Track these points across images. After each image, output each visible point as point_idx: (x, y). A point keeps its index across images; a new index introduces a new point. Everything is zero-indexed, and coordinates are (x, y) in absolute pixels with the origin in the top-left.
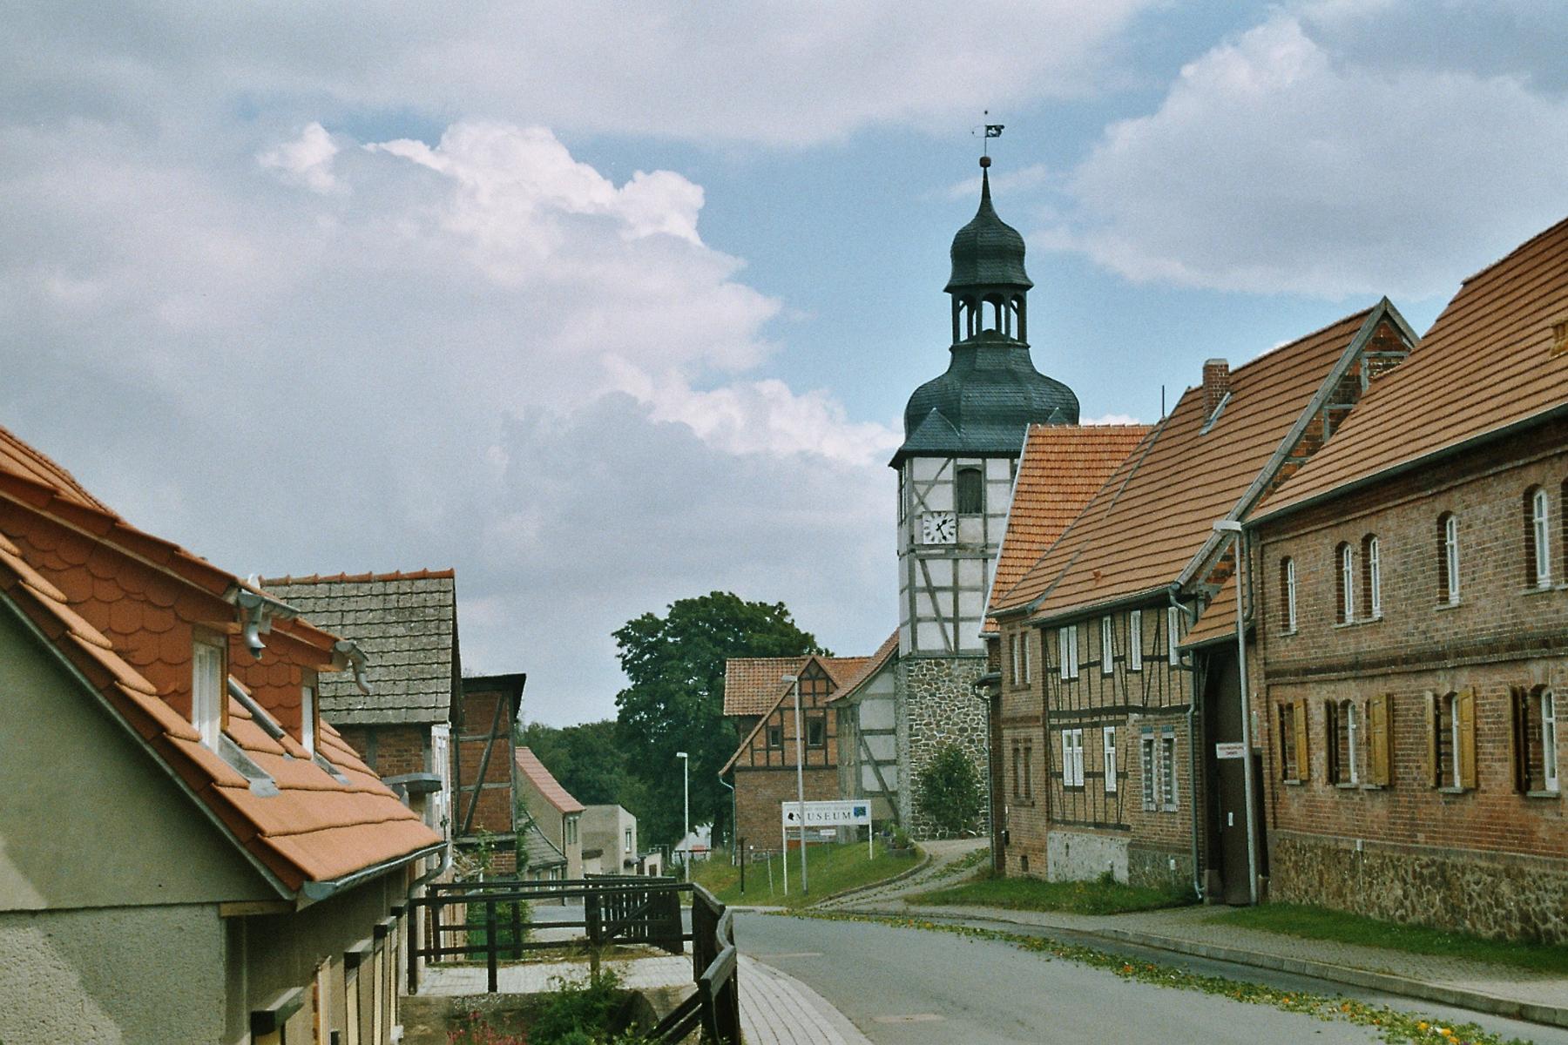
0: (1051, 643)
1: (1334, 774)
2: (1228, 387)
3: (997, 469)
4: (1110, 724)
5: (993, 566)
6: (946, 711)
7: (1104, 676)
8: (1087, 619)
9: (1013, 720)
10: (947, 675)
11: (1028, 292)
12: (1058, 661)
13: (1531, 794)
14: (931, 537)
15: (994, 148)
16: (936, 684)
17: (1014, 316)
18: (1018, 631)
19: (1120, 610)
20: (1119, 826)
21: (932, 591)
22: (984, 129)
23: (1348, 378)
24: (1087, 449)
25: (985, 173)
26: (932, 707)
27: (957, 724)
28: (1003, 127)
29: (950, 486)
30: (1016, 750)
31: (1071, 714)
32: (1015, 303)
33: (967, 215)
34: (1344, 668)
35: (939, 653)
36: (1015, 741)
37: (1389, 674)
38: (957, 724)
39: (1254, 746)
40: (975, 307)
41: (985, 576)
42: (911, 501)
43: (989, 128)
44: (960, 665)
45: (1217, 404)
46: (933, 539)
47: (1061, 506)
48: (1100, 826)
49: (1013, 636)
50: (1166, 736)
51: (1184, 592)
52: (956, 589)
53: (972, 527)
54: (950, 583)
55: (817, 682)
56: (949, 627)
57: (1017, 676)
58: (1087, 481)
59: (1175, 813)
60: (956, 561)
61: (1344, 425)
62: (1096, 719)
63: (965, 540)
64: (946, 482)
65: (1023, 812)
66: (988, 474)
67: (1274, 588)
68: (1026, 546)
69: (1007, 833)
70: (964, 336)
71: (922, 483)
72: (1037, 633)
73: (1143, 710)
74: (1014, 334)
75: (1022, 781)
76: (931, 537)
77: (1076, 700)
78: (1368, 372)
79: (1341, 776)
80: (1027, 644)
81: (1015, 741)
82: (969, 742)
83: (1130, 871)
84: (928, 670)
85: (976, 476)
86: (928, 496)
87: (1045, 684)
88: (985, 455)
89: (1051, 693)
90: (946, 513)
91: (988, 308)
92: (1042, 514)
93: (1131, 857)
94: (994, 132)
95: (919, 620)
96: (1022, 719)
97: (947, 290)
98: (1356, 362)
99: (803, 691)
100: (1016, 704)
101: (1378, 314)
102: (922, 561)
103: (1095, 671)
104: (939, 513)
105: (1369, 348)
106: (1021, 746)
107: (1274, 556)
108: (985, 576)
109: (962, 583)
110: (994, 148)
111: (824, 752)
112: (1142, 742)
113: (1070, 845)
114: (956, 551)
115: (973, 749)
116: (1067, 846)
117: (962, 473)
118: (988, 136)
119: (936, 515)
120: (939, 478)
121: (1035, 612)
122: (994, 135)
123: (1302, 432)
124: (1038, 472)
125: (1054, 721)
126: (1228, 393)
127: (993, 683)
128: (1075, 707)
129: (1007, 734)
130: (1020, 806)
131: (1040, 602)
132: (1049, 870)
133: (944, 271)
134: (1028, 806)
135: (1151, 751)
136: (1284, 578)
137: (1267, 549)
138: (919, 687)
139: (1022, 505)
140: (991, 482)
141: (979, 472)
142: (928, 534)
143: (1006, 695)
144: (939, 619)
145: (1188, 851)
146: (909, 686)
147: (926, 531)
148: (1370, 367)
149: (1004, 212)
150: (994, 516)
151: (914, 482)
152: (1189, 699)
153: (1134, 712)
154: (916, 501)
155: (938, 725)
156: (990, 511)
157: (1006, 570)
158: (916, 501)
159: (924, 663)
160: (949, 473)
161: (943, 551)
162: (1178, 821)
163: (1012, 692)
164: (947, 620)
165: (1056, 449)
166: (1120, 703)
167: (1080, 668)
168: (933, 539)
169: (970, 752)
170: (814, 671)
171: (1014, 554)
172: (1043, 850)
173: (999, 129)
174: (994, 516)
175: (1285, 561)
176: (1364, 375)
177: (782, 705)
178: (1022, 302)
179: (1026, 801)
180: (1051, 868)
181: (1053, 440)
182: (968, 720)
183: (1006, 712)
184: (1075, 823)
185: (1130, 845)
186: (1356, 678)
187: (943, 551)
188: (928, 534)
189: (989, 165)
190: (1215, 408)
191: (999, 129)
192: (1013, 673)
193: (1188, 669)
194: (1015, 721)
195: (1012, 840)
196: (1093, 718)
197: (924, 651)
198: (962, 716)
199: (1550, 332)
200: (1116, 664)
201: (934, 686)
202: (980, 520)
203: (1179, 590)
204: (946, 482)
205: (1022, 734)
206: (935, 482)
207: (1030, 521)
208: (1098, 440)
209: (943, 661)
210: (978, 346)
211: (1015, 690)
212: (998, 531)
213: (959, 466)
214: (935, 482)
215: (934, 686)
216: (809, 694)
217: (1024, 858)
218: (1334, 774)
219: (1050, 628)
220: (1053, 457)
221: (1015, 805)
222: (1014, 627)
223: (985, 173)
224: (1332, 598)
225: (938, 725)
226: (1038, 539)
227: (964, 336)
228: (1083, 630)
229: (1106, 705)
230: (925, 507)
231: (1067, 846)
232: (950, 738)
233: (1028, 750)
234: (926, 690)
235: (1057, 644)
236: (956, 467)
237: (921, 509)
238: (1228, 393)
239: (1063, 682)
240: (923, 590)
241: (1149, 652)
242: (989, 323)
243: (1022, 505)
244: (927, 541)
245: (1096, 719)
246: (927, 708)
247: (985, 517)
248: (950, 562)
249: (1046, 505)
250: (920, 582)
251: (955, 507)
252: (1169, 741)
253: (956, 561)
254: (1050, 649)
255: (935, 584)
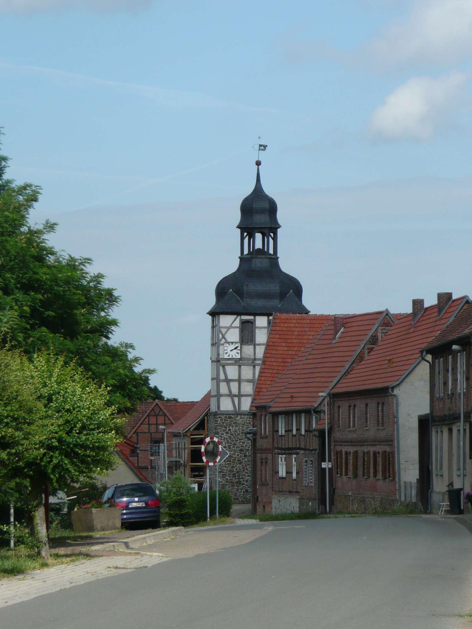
0: (276, 421)
1: (375, 475)
2: (343, 325)
3: (261, 321)
4: (295, 454)
5: (258, 369)
6: (233, 441)
7: (293, 436)
8: (288, 414)
9: (261, 450)
10: (234, 423)
11: (278, 229)
12: (278, 428)
13: (377, 478)
14: (228, 355)
15: (263, 156)
16: (229, 427)
17: (271, 241)
18: (264, 414)
19: (298, 413)
20: (297, 492)
21: (228, 381)
22: (258, 146)
23: (374, 336)
24: (300, 325)
25: (258, 169)
26: (227, 439)
27: (239, 447)
28: (267, 146)
29: (238, 330)
30: (262, 462)
31: (281, 449)
32: (272, 234)
33: (249, 189)
34: (348, 442)
35: (231, 412)
36: (261, 459)
37: (364, 445)
38: (239, 447)
39: (136, 458)
40: (251, 236)
41: (254, 374)
42: (218, 337)
43: (261, 146)
44: (241, 418)
45: (339, 332)
46: (229, 356)
47: (287, 353)
48: (290, 492)
49: (261, 415)
50: (311, 459)
51: (316, 410)
52: (239, 381)
53: (248, 350)
54: (236, 377)
55: (158, 417)
56: (236, 399)
57: (263, 432)
58: (299, 341)
59: (313, 486)
60: (240, 366)
61: (372, 353)
62: (290, 452)
63: (244, 356)
64: (236, 327)
65: (264, 488)
66: (256, 324)
67: (336, 415)
68: (271, 371)
69: (258, 497)
70: (246, 252)
71: (225, 327)
72: (271, 415)
73: (305, 449)
74: (271, 251)
75: (263, 475)
76: (228, 355)
77: (283, 444)
78: (381, 334)
79: (348, 474)
80: (267, 418)
81: (261, 459)
82: (244, 456)
83: (299, 508)
84: (225, 420)
85: (250, 324)
86: (227, 334)
87: (273, 436)
88: (255, 315)
89: (275, 440)
90: (236, 343)
91: (259, 236)
92: (278, 356)
93: (300, 503)
94: (263, 148)
95: (221, 395)
96: (264, 450)
97: (238, 227)
98: (376, 330)
99: (150, 422)
100: (261, 443)
101: (385, 314)
102: (223, 366)
103: (290, 433)
104: (232, 343)
105: (382, 326)
106: (264, 461)
107: (336, 405)
108: (254, 374)
109: (243, 377)
110: (263, 156)
111: (136, 458)
112: (304, 461)
113: (281, 500)
114: (239, 362)
115: (246, 460)
116: (279, 501)
117: (243, 323)
118: (260, 150)
119: (231, 344)
120: (232, 326)
121: (270, 407)
122: (263, 150)
123: (358, 355)
124: (277, 336)
125: (276, 451)
126: (343, 328)
127: (255, 434)
128: (283, 447)
129: (259, 456)
130: (263, 485)
131: (272, 403)
132: (273, 510)
133: (237, 217)
134: (266, 485)
135: (307, 464)
136: (339, 412)
137: (336, 402)
138: (220, 429)
139: (270, 352)
140: (258, 328)
141: (252, 323)
142: (226, 353)
143: (258, 439)
144: (231, 395)
145: (316, 500)
146: (215, 428)
147: (226, 352)
148: (381, 333)
149: (268, 190)
150: (259, 345)
151: (220, 327)
152: (317, 447)
153: (302, 450)
154: (221, 336)
155: (229, 448)
156: (257, 342)
157: (261, 382)
158: (221, 336)
159: (223, 417)
160: (237, 323)
161: (233, 362)
162: (314, 489)
163: (261, 438)
164: (235, 396)
165: (286, 325)
166: (298, 446)
167: (285, 431)
168: (229, 356)
169: (245, 461)
170: (157, 411)
171: (266, 374)
172: (271, 503)
173: (265, 147)
174: (259, 345)
175: (339, 407)
176: (379, 335)
177: (138, 431)
178: (275, 234)
179: (264, 484)
180: (273, 510)
181: (284, 321)
182: (244, 445)
183: (258, 445)
184: (282, 492)
185: (299, 499)
186: (351, 445)
187: (233, 362)
188: (226, 353)
189: (260, 165)
190: (338, 333)
191: (265, 147)
192: (261, 430)
193: (316, 437)
194: (263, 451)
195: (260, 499)
196: (288, 451)
197: (223, 411)
198: (241, 444)
199: (387, 362)
200: (297, 432)
201: (228, 428)
202: (252, 347)
203: (315, 409)
204: (236, 327)
205: (264, 456)
206: (231, 327)
207: (273, 360)
208: (305, 321)
209: (233, 416)
210: (253, 258)
211: (262, 438)
212: (260, 352)
213: (243, 319)
214: (231, 327)
215: (228, 428)
216: (154, 424)
217: (264, 506)
218: (346, 474)
219: (275, 415)
220: (284, 329)
221: (261, 485)
222: (262, 412)
223: (258, 169)
224: (347, 420)
225: (229, 448)
226: (276, 368)
227: (246, 252)
228: (287, 417)
229: (293, 446)
230: (225, 339)
231: (279, 501)
232: (235, 454)
233: (266, 462)
234: (224, 430)
235: (278, 422)
236: (241, 320)
237: (223, 341)
238: (343, 328)
239: (280, 436)
240: (224, 381)
241: (307, 429)
242: (259, 245)
243: (270, 352)
244: (226, 356)
245: (290, 452)
246: (224, 439)
247: (255, 345)
248: (237, 367)
249: (280, 352)
250: (222, 377)
251: (240, 340)
252: (312, 461)
253: (240, 366)
254: (275, 422)
255: (230, 377)
